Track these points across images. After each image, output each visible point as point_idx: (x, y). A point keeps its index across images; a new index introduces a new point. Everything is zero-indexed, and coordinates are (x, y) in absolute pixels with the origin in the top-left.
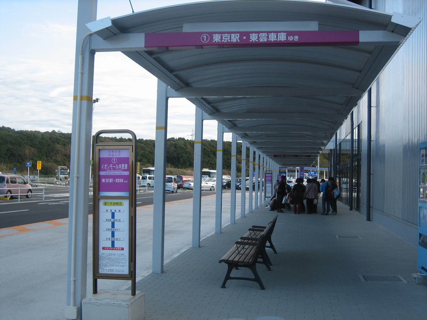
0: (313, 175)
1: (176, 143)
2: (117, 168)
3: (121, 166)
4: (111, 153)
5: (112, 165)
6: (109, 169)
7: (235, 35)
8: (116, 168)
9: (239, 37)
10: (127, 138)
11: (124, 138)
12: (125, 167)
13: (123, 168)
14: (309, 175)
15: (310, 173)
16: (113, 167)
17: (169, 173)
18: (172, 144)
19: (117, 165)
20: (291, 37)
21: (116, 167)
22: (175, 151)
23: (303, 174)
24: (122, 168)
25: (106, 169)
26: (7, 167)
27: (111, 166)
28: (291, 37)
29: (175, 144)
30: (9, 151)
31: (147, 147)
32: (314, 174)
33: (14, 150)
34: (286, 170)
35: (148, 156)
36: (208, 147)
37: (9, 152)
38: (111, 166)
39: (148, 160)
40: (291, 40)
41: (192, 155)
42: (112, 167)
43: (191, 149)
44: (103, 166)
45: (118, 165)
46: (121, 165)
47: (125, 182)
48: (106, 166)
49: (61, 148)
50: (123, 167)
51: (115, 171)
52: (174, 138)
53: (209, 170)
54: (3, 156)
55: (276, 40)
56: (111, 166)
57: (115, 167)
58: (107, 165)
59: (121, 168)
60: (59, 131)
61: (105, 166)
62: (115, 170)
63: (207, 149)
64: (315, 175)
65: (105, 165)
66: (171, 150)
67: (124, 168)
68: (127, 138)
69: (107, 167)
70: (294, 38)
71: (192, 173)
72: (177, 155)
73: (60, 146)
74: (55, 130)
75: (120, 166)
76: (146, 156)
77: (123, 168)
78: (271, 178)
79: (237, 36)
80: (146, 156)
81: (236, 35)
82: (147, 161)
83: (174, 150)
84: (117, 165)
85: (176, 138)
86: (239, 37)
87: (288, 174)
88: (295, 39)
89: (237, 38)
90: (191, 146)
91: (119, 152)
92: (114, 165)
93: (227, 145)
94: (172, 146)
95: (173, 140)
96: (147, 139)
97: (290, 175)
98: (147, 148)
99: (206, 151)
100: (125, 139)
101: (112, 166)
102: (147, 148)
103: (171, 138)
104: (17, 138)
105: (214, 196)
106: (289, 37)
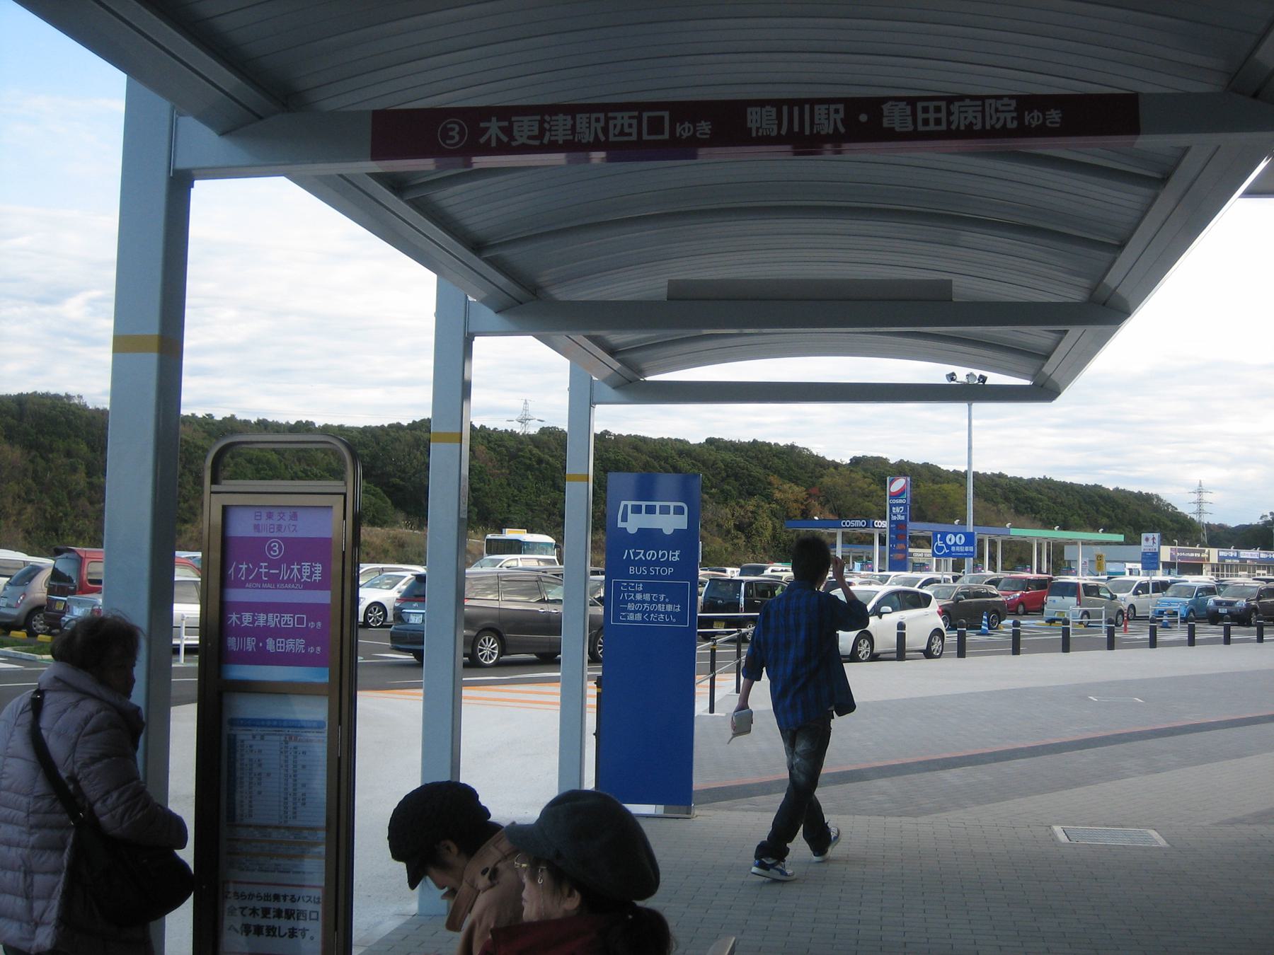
0: (962, 549)
2: (285, 578)
3: (300, 571)
4: (264, 521)
5: (266, 564)
6: (254, 580)
7: (590, 118)
9: (842, 115)
10: (253, 420)
12: (312, 573)
13: (308, 577)
14: (940, 549)
15: (945, 542)
16: (271, 571)
19: (284, 566)
23: (905, 551)
24: (302, 578)
25: (243, 579)
27: (263, 570)
32: (964, 545)
36: (555, 453)
38: (260, 570)
40: (685, 135)
41: (492, 482)
42: (265, 572)
48: (244, 569)
53: (527, 532)
55: (571, 137)
56: (260, 570)
57: (278, 571)
61: (242, 568)
62: (276, 586)
63: (551, 459)
64: (967, 549)
69: (249, 571)
70: (697, 128)
75: (296, 570)
77: (305, 578)
79: (837, 111)
81: (594, 116)
84: (284, 566)
87: (846, 549)
88: (701, 134)
89: (835, 119)
90: (490, 448)
91: (291, 519)
92: (274, 564)
93: (627, 449)
94: (418, 446)
96: (330, 423)
97: (854, 554)
99: (544, 465)
100: (247, 423)
101: (265, 568)
106: (680, 126)
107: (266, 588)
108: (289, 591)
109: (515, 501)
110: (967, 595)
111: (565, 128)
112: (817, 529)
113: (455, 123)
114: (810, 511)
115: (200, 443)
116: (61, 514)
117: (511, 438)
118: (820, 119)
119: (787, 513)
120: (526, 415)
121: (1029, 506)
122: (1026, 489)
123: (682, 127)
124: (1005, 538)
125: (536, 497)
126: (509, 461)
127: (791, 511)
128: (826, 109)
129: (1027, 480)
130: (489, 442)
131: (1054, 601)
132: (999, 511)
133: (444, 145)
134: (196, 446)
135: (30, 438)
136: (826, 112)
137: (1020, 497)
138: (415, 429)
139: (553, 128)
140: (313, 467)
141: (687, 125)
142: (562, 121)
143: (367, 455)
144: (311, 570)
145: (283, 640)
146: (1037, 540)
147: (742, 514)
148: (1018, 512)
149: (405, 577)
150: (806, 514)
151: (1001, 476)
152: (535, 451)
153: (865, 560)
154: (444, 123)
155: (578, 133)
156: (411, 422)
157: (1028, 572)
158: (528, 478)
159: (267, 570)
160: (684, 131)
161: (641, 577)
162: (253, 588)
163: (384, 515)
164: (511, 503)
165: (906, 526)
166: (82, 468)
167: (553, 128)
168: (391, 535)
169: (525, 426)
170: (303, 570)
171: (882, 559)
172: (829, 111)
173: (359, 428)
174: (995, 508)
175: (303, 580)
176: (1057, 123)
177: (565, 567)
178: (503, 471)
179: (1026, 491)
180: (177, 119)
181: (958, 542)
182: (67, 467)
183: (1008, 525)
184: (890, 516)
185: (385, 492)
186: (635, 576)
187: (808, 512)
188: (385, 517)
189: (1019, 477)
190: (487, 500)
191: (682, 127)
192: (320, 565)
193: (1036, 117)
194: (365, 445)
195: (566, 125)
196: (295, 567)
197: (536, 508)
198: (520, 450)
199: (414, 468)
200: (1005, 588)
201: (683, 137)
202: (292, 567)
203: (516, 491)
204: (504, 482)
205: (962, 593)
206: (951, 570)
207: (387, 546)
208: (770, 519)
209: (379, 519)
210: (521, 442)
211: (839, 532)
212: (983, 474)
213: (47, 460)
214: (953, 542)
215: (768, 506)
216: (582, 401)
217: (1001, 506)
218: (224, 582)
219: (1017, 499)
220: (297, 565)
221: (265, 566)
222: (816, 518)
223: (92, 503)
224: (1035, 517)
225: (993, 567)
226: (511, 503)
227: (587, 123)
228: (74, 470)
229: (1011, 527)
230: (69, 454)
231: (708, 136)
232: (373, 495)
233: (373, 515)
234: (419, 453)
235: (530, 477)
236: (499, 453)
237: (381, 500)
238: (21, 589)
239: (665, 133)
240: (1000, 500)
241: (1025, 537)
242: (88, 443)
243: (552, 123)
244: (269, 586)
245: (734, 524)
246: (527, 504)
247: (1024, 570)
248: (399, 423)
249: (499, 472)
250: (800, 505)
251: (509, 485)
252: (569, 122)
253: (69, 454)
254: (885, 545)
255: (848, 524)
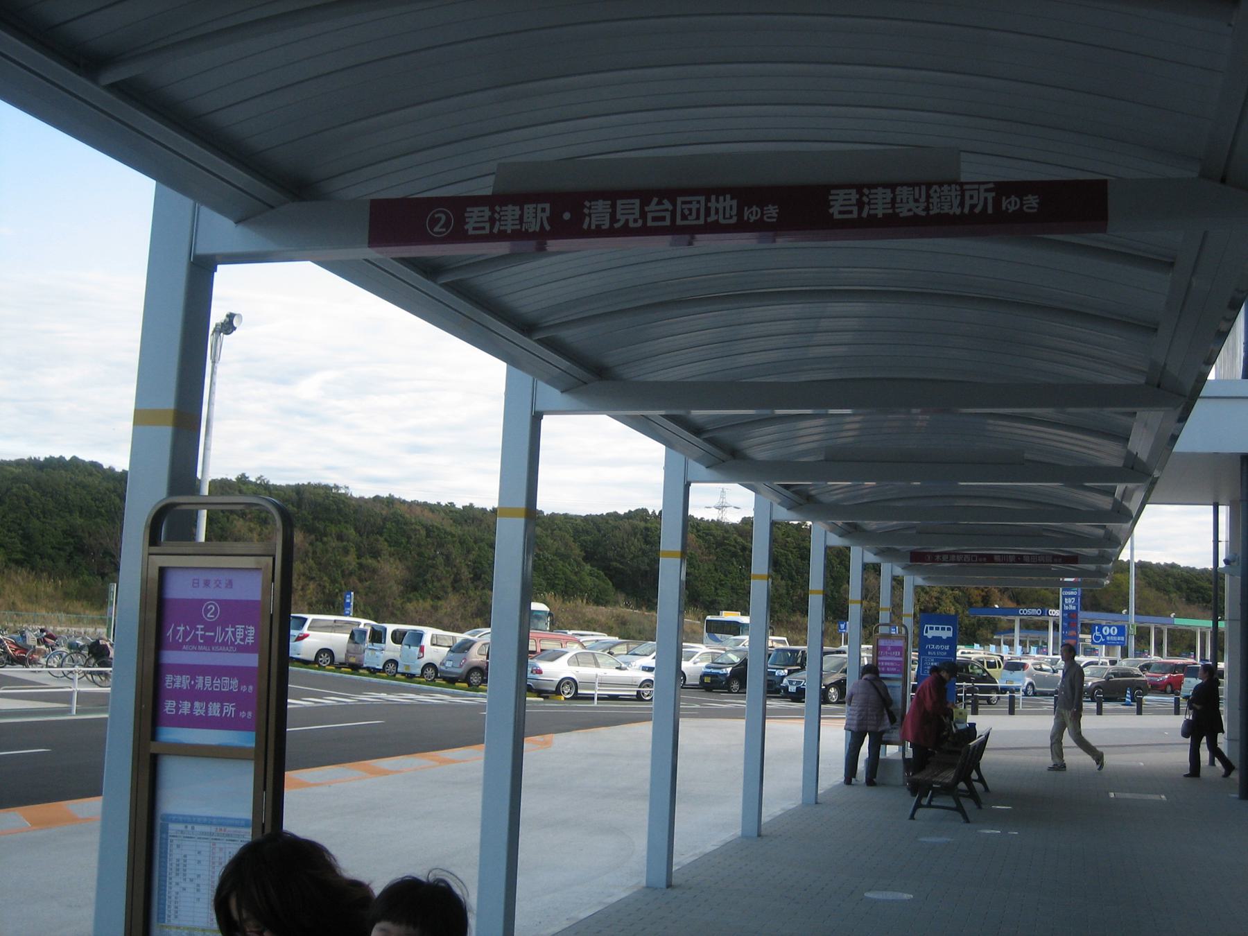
0: (1115, 638)
1: (649, 525)
2: (220, 641)
3: (234, 633)
5: (202, 626)
6: (191, 643)
7: (536, 208)
8: (216, 641)
9: (548, 213)
11: (480, 506)
12: (245, 635)
13: (241, 640)
14: (1097, 638)
15: (1102, 633)
16: (207, 634)
17: (614, 626)
18: (634, 528)
19: (219, 629)
20: (1013, 198)
21: (215, 635)
22: (644, 553)
23: (1076, 637)
24: (236, 641)
25: (180, 641)
26: (56, 588)
27: (200, 633)
28: (1013, 198)
29: (647, 529)
30: (73, 537)
31: (549, 538)
32: (1118, 635)
33: (87, 535)
34: (1014, 621)
35: (551, 565)
37: (72, 540)
38: (197, 633)
39: (548, 579)
40: (1012, 209)
41: (701, 567)
43: (700, 547)
44: (171, 630)
45: (223, 630)
46: (233, 629)
47: (244, 688)
48: (181, 631)
49: (251, 530)
50: (239, 637)
51: (211, 651)
52: (645, 511)
53: (741, 615)
54: (50, 551)
55: (519, 227)
56: (197, 633)
57: (212, 634)
58: (185, 626)
59: (233, 640)
60: (262, 476)
61: (179, 630)
62: (211, 649)
64: (1119, 638)
65: (178, 628)
66: (629, 549)
67: (242, 640)
68: (491, 508)
69: (186, 634)
71: (695, 628)
72: (648, 564)
73: (248, 523)
74: (247, 475)
75: (230, 633)
76: (545, 566)
77: (238, 641)
78: (901, 659)
80: (542, 568)
82: (544, 583)
83: (641, 549)
84: (219, 629)
85: (654, 512)
86: (548, 215)
87: (1024, 634)
90: (699, 536)
92: (210, 627)
94: (635, 534)
95: (642, 516)
97: (1032, 639)
98: (550, 541)
101: (201, 630)
102: (550, 541)
103: (637, 510)
104: (106, 494)
105: (644, 730)
107: (201, 651)
108: (222, 654)
109: (721, 585)
110: (1116, 675)
111: (885, 201)
112: (991, 616)
113: (437, 212)
114: (990, 598)
115: (448, 529)
116: (337, 590)
117: (718, 527)
118: (528, 218)
119: (969, 599)
120: (723, 502)
121: (1200, 595)
122: (1197, 579)
123: (1007, 201)
124: (1170, 627)
125: (740, 581)
126: (717, 548)
127: (973, 597)
128: (534, 208)
129: (1199, 570)
130: (698, 531)
131: (1189, 682)
132: (1170, 599)
133: (431, 233)
134: (445, 533)
135: (308, 523)
136: (534, 210)
137: (1191, 586)
138: (631, 518)
139: (872, 201)
140: (545, 552)
141: (754, 208)
142: (511, 212)
143: (590, 541)
144: (244, 632)
145: (223, 690)
146: (1201, 629)
147: (927, 599)
148: (1189, 600)
149: (697, 652)
150: (986, 601)
151: (1173, 566)
152: (740, 540)
153: (1040, 644)
154: (431, 214)
155: (526, 223)
156: (627, 511)
157: (1191, 658)
158: (733, 564)
159: (203, 633)
160: (1011, 205)
161: (933, 656)
162: (189, 651)
163: (607, 596)
164: (718, 586)
165: (1077, 615)
166: (353, 550)
167: (872, 201)
168: (615, 615)
169: (722, 512)
170: (237, 633)
171: (1055, 643)
172: (536, 216)
173: (581, 516)
174: (1167, 597)
175: (236, 643)
176: (774, 218)
177: (657, 643)
178: (711, 557)
179: (1198, 582)
180: (198, 208)
181: (1112, 633)
182: (340, 550)
183: (1172, 615)
184: (1063, 606)
185: (606, 575)
186: (930, 656)
187: (987, 598)
188: (607, 598)
189: (1191, 567)
190: (698, 584)
191: (1007, 201)
192: (253, 628)
193: (1013, 202)
194: (587, 532)
195: (885, 198)
196: (230, 630)
197: (740, 591)
198: (724, 538)
199: (632, 553)
200: (1156, 671)
201: (751, 221)
202: (227, 629)
203: (722, 575)
204: (712, 568)
205: (1112, 673)
206: (1051, 654)
207: (611, 623)
208: (953, 605)
209: (602, 599)
210: (727, 531)
211: (1017, 620)
212: (1157, 564)
213: (324, 543)
214: (1108, 633)
215: (951, 592)
216: (679, 490)
217: (1173, 595)
218: (160, 644)
219: (1188, 588)
220: (232, 627)
221: (201, 629)
222: (997, 606)
223: (361, 580)
224: (1206, 606)
225: (1159, 652)
226: (718, 586)
227: (534, 213)
228: (346, 551)
229: (1175, 617)
230: (340, 537)
231: (1035, 210)
232: (597, 577)
233: (597, 596)
234: (636, 540)
235: (735, 563)
236: (705, 541)
237: (604, 582)
238: (462, 655)
239: (701, 218)
240: (1171, 589)
241: (1189, 626)
242: (356, 529)
243: (871, 197)
244: (205, 648)
245: (920, 609)
246: (732, 588)
247: (1188, 656)
248: (616, 512)
249: (707, 558)
250: (980, 592)
251: (716, 570)
252: (518, 212)
253: (340, 537)
254: (1058, 631)
255: (1025, 612)
